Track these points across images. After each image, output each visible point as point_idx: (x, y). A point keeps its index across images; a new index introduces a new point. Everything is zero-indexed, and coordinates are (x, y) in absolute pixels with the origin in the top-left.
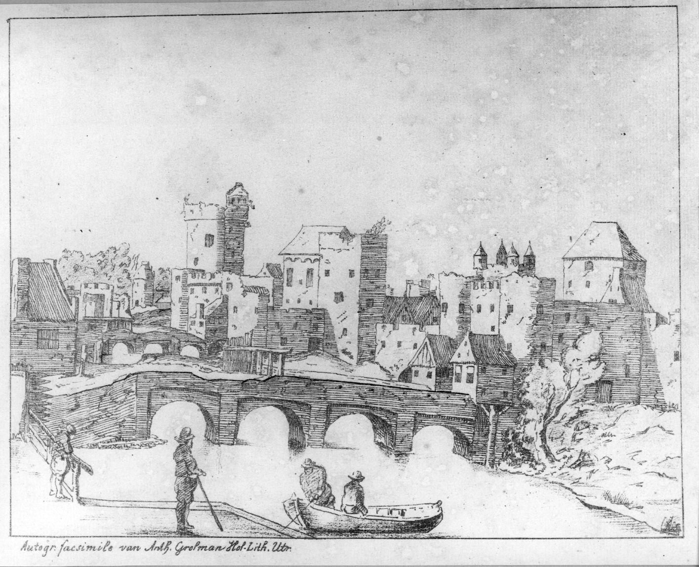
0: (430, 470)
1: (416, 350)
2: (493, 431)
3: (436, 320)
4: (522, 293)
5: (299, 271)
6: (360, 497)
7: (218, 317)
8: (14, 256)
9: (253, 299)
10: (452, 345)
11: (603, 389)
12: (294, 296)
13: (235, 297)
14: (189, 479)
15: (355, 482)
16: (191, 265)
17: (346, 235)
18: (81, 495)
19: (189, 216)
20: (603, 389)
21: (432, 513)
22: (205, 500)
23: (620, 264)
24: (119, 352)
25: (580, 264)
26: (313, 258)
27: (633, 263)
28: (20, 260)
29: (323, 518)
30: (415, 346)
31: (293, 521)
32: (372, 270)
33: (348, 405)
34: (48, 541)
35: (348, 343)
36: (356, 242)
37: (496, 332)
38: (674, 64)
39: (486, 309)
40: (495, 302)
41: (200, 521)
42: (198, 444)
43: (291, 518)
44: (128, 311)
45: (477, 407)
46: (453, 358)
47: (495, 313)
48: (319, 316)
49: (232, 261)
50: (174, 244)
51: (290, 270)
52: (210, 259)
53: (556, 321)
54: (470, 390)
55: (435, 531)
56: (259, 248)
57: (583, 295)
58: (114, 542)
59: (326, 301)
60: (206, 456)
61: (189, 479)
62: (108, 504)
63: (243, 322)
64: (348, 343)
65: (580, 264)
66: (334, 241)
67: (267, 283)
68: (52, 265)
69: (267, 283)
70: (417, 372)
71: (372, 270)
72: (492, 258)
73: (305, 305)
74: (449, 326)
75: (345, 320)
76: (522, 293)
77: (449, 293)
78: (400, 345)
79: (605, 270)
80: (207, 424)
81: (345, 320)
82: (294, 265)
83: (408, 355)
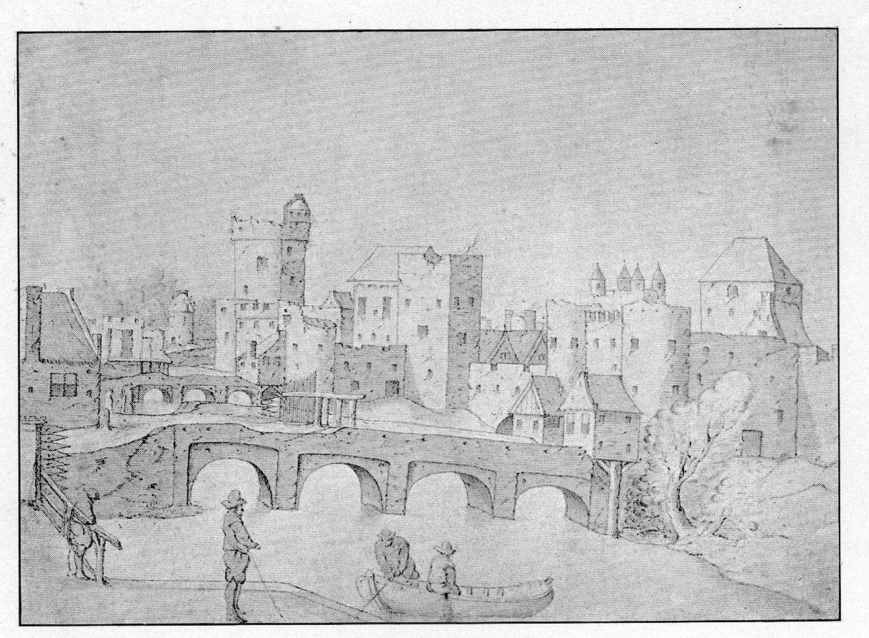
3: (544, 358)
4: (651, 327)
5: (374, 301)
9: (316, 333)
12: (366, 330)
14: (240, 550)
17: (432, 257)
25: (722, 288)
32: (467, 298)
35: (434, 393)
36: (444, 268)
38: (529, 495)
45: (596, 463)
47: (617, 351)
48: (396, 354)
54: (588, 444)
56: (323, 270)
57: (729, 327)
60: (265, 526)
64: (434, 393)
68: (69, 296)
71: (467, 298)
72: (612, 283)
73: (381, 342)
74: (559, 363)
75: (429, 358)
77: (562, 330)
78: (497, 392)
79: (755, 295)
81: (429, 358)
82: (368, 293)
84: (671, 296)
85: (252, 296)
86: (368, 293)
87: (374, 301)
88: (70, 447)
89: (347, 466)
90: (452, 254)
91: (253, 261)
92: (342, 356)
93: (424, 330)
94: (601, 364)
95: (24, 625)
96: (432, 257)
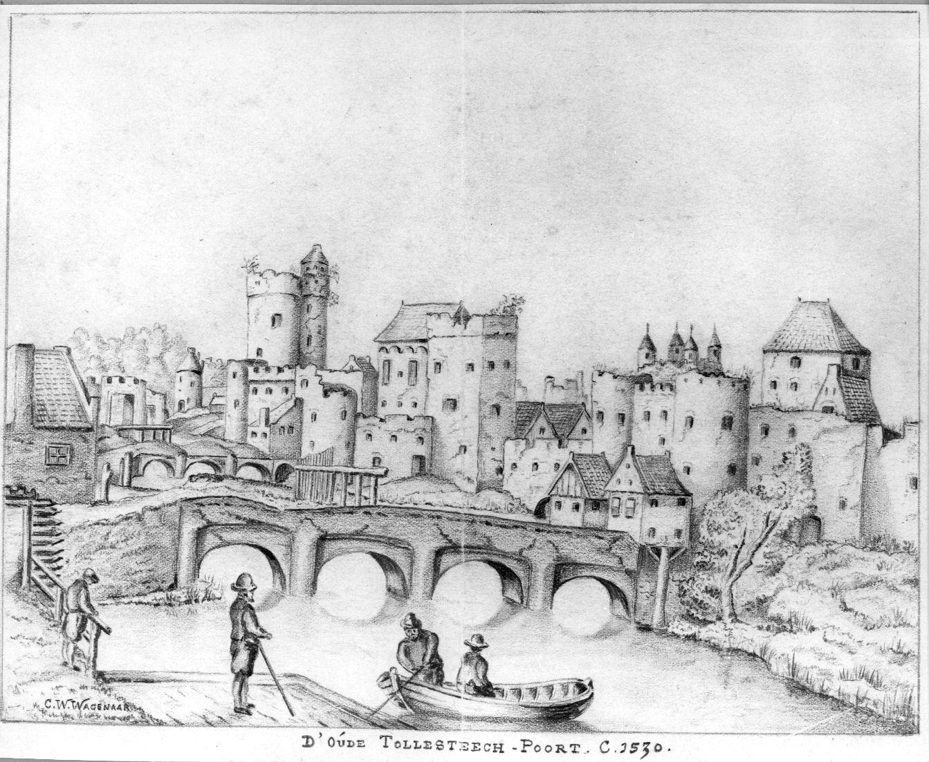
0: (563, 639)
2: (675, 583)
4: (703, 398)
13: (312, 395)
16: (253, 356)
17: (461, 317)
18: (100, 668)
21: (572, 697)
24: (154, 474)
30: (557, 466)
34: (401, 374)
46: (610, 484)
56: (351, 331)
58: (60, 719)
65: (785, 359)
66: (442, 326)
67: (354, 382)
69: (354, 382)
70: (559, 505)
74: (603, 440)
76: (703, 398)
77: (606, 395)
93: (453, 404)
94: (647, 444)
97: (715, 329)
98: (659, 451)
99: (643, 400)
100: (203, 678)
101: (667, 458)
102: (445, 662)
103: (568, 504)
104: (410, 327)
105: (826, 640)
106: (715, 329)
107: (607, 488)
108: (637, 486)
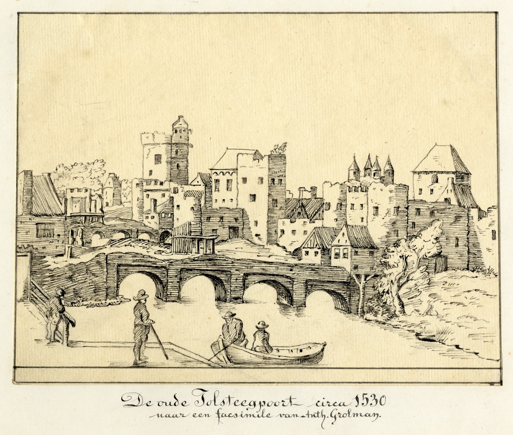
1: (306, 236)
5: (223, 180)
6: (266, 340)
7: (168, 214)
8: (20, 170)
10: (335, 232)
11: (440, 261)
13: (178, 199)
14: (145, 327)
15: (262, 329)
16: (147, 176)
17: (257, 156)
19: (145, 141)
20: (440, 261)
22: (157, 341)
23: (454, 176)
25: (429, 178)
26: (231, 172)
27: (462, 176)
28: (26, 172)
29: (241, 354)
31: (215, 355)
32: (275, 181)
33: (194, 269)
37: (364, 224)
39: (357, 206)
40: (364, 202)
41: (152, 355)
42: (151, 301)
43: (227, 352)
44: (101, 210)
49: (179, 174)
50: (134, 162)
51: (217, 181)
52: (161, 172)
53: (409, 217)
55: (323, 363)
56: (197, 165)
59: (244, 203)
61: (145, 327)
62: (90, 344)
63: (184, 216)
65: (429, 178)
66: (247, 160)
71: (275, 181)
74: (329, 218)
75: (258, 213)
76: (382, 195)
77: (332, 196)
80: (279, 294)
81: (258, 213)
82: (220, 177)
83: (299, 240)
84: (398, 179)
85: (153, 177)
86: (220, 177)
87: (223, 180)
88: (453, 150)
89: (140, 274)
90: (287, 145)
91: (152, 158)
92: (202, 213)
93: (254, 197)
94: (354, 217)
95: (16, 259)
96: (257, 156)
97: (389, 157)
98: (359, 223)
99: (351, 197)
100: (112, 344)
101: (364, 228)
102: (341, 316)
103: (312, 252)
104: (228, 163)
105: (123, 400)
106: (389, 157)
107: (333, 243)
108: (348, 243)
